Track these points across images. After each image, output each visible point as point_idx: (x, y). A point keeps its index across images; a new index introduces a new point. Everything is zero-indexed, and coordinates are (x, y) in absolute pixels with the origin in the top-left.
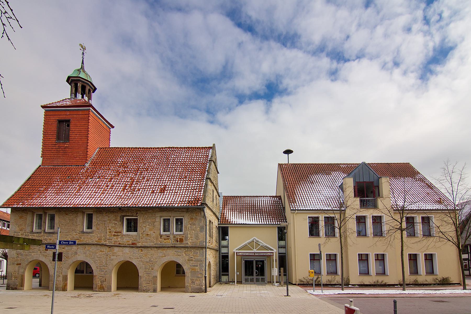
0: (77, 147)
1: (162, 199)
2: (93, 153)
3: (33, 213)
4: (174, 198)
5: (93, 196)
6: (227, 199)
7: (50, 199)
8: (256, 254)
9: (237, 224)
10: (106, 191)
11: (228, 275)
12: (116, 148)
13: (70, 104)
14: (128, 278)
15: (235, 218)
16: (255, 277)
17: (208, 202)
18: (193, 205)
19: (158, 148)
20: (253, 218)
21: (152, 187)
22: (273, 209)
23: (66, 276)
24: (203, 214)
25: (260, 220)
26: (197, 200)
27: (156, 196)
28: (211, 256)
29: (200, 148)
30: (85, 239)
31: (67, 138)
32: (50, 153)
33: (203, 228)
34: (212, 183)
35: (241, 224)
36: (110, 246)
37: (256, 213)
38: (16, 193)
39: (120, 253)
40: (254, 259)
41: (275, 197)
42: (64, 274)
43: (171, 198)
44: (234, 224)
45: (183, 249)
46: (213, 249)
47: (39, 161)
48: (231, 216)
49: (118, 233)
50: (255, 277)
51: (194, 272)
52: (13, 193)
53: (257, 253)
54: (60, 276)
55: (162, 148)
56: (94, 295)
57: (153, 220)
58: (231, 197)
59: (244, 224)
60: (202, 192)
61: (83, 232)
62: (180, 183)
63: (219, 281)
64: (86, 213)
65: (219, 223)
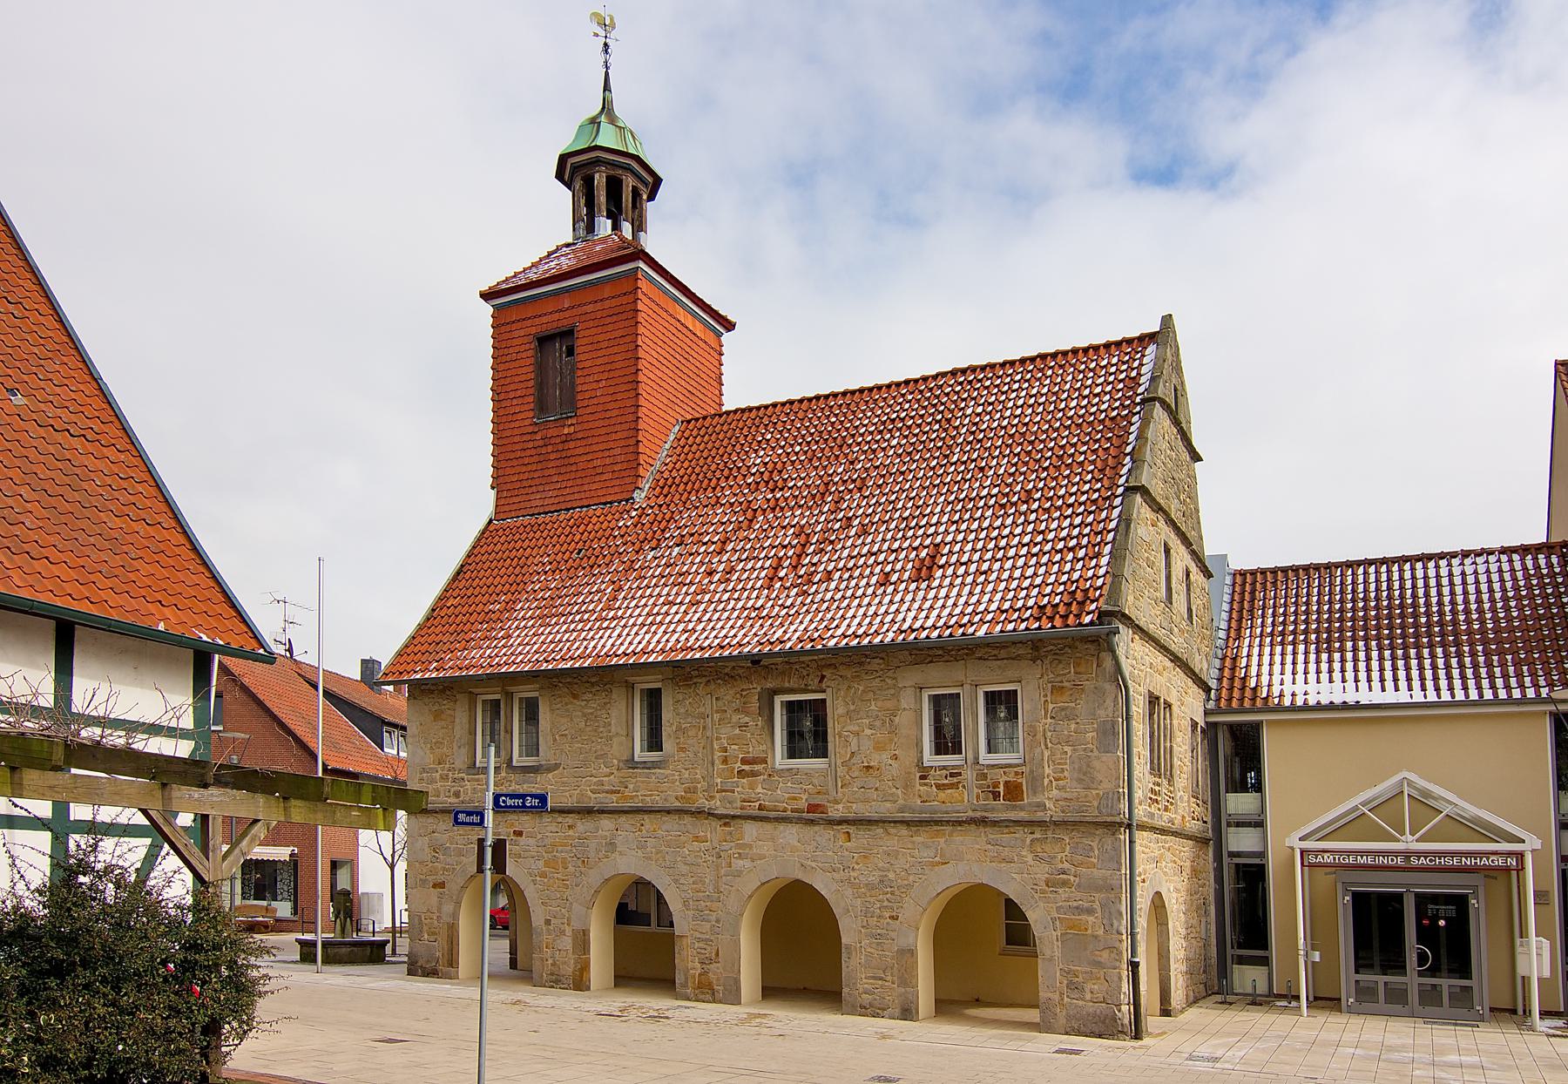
0: (603, 431)
1: (920, 609)
2: (659, 448)
3: (473, 698)
4: (974, 600)
5: (659, 618)
6: (1252, 587)
7: (522, 644)
8: (1414, 862)
9: (1306, 708)
10: (704, 592)
11: (1265, 962)
12: (743, 411)
13: (573, 262)
14: (803, 957)
15: (1292, 679)
16: (1412, 979)
17: (1140, 603)
18: (1058, 622)
19: (907, 382)
20: (1402, 674)
21: (881, 558)
22: (1523, 619)
23: (586, 933)
24: (1108, 663)
25: (1443, 683)
26: (1078, 598)
27: (898, 598)
28: (1167, 866)
29: (1096, 348)
30: (642, 790)
31: (570, 403)
32: (517, 470)
33: (1115, 734)
34: (1158, 508)
35: (1331, 707)
36: (727, 819)
37: (1418, 646)
38: (420, 627)
39: (766, 848)
40: (1410, 887)
41: (1538, 548)
42: (576, 925)
43: (962, 601)
44: (1293, 708)
45: (1020, 832)
46: (1175, 834)
47: (480, 505)
48: (1277, 668)
49: (753, 765)
50: (1412, 979)
51: (1075, 938)
52: (409, 627)
53: (1419, 854)
54: (563, 932)
55: (925, 379)
56: (677, 1013)
57: (889, 704)
58: (1274, 571)
59: (1345, 706)
60: (1104, 561)
61: (631, 763)
62: (1003, 525)
63: (1214, 985)
64: (638, 687)
65: (1211, 705)
